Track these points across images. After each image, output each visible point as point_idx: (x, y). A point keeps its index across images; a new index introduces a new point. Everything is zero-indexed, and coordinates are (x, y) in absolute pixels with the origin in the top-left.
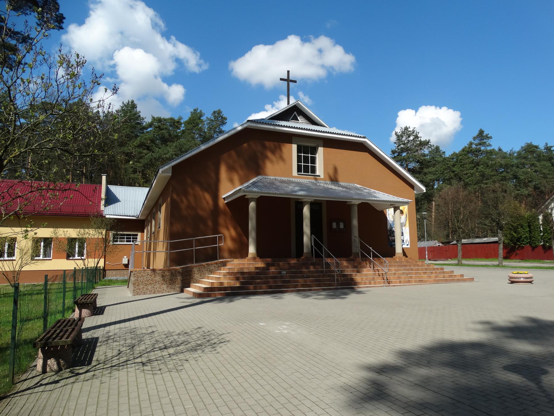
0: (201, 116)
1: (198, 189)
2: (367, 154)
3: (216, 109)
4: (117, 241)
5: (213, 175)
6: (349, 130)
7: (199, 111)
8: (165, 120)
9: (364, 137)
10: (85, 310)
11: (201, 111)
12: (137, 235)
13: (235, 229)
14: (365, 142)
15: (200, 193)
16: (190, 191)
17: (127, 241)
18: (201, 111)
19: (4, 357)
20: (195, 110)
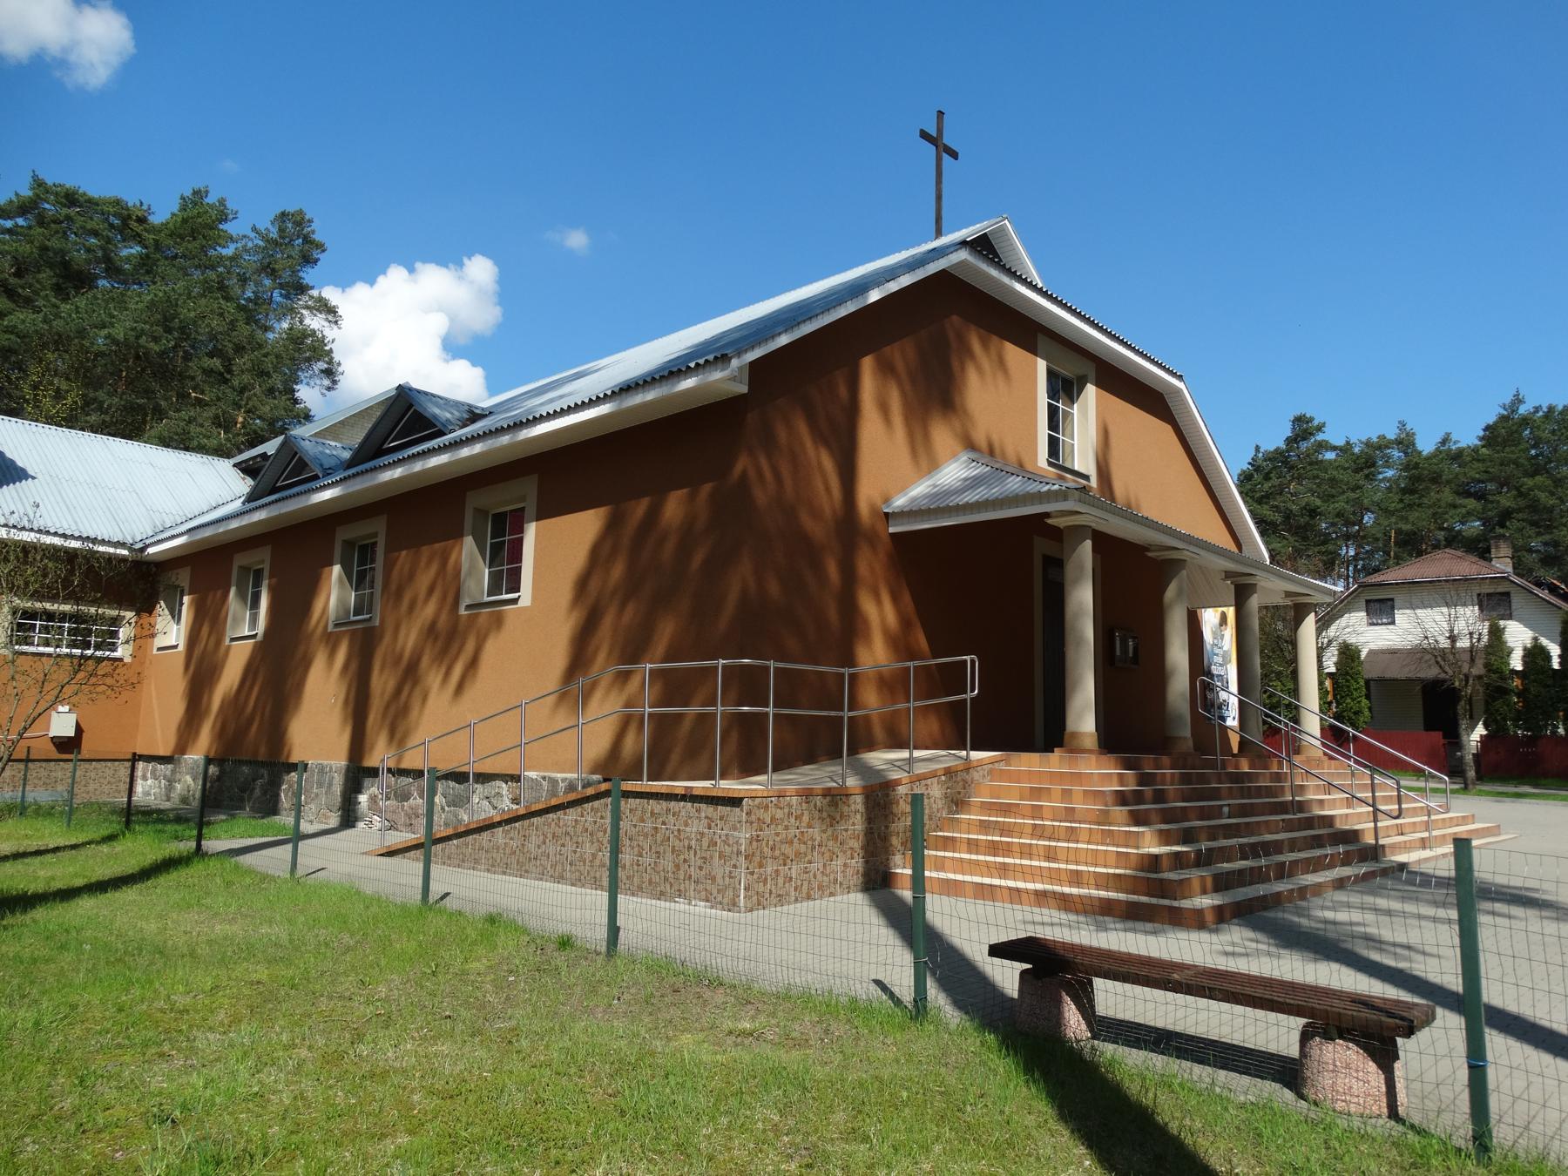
0: (223, 217)
1: (802, 428)
2: (1167, 429)
3: (291, 208)
4: (27, 641)
5: (843, 391)
6: (526, 383)
7: (211, 199)
8: (92, 202)
9: (1180, 378)
10: (1210, 610)
11: (222, 202)
12: (116, 621)
13: (895, 599)
14: (1179, 391)
15: (809, 444)
16: (782, 435)
17: (73, 645)
18: (222, 202)
19: (47, 1080)
20: (196, 193)
